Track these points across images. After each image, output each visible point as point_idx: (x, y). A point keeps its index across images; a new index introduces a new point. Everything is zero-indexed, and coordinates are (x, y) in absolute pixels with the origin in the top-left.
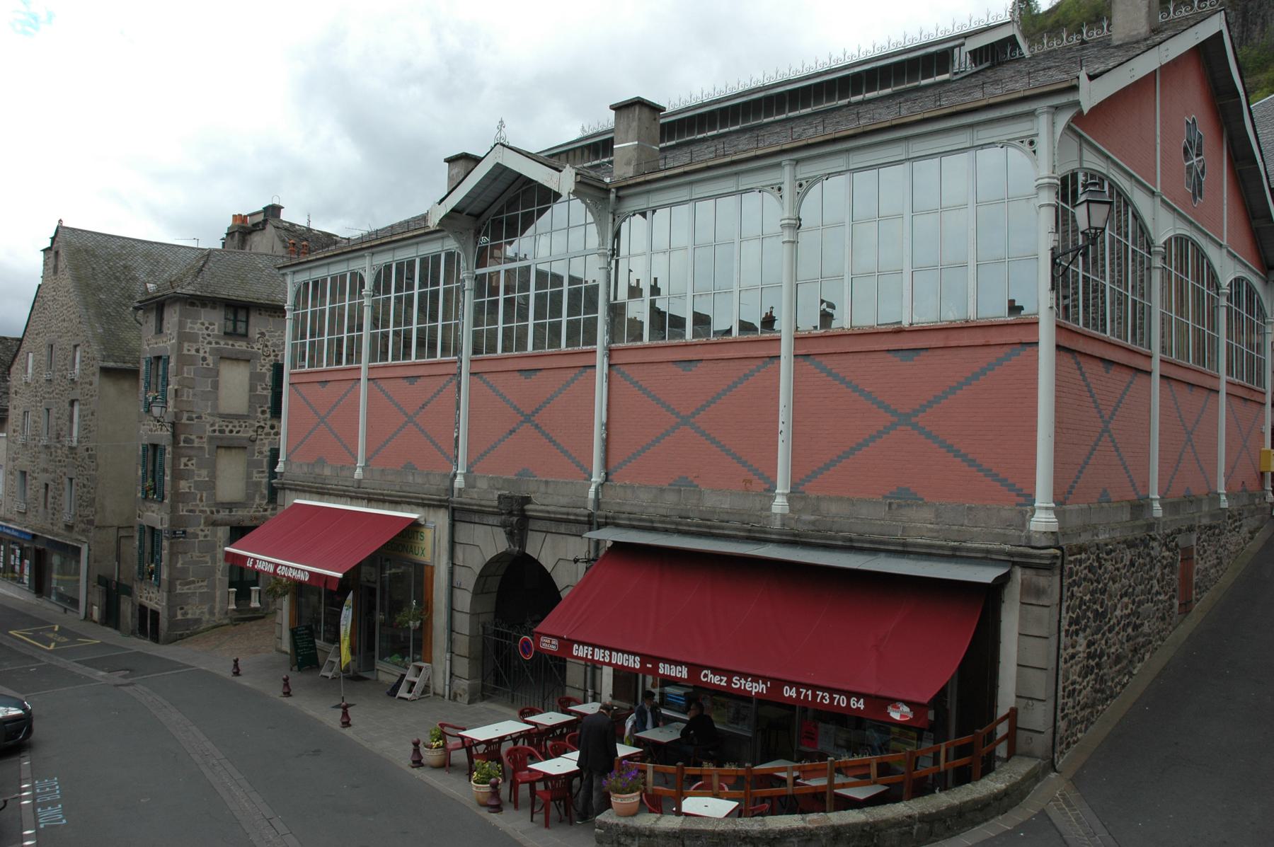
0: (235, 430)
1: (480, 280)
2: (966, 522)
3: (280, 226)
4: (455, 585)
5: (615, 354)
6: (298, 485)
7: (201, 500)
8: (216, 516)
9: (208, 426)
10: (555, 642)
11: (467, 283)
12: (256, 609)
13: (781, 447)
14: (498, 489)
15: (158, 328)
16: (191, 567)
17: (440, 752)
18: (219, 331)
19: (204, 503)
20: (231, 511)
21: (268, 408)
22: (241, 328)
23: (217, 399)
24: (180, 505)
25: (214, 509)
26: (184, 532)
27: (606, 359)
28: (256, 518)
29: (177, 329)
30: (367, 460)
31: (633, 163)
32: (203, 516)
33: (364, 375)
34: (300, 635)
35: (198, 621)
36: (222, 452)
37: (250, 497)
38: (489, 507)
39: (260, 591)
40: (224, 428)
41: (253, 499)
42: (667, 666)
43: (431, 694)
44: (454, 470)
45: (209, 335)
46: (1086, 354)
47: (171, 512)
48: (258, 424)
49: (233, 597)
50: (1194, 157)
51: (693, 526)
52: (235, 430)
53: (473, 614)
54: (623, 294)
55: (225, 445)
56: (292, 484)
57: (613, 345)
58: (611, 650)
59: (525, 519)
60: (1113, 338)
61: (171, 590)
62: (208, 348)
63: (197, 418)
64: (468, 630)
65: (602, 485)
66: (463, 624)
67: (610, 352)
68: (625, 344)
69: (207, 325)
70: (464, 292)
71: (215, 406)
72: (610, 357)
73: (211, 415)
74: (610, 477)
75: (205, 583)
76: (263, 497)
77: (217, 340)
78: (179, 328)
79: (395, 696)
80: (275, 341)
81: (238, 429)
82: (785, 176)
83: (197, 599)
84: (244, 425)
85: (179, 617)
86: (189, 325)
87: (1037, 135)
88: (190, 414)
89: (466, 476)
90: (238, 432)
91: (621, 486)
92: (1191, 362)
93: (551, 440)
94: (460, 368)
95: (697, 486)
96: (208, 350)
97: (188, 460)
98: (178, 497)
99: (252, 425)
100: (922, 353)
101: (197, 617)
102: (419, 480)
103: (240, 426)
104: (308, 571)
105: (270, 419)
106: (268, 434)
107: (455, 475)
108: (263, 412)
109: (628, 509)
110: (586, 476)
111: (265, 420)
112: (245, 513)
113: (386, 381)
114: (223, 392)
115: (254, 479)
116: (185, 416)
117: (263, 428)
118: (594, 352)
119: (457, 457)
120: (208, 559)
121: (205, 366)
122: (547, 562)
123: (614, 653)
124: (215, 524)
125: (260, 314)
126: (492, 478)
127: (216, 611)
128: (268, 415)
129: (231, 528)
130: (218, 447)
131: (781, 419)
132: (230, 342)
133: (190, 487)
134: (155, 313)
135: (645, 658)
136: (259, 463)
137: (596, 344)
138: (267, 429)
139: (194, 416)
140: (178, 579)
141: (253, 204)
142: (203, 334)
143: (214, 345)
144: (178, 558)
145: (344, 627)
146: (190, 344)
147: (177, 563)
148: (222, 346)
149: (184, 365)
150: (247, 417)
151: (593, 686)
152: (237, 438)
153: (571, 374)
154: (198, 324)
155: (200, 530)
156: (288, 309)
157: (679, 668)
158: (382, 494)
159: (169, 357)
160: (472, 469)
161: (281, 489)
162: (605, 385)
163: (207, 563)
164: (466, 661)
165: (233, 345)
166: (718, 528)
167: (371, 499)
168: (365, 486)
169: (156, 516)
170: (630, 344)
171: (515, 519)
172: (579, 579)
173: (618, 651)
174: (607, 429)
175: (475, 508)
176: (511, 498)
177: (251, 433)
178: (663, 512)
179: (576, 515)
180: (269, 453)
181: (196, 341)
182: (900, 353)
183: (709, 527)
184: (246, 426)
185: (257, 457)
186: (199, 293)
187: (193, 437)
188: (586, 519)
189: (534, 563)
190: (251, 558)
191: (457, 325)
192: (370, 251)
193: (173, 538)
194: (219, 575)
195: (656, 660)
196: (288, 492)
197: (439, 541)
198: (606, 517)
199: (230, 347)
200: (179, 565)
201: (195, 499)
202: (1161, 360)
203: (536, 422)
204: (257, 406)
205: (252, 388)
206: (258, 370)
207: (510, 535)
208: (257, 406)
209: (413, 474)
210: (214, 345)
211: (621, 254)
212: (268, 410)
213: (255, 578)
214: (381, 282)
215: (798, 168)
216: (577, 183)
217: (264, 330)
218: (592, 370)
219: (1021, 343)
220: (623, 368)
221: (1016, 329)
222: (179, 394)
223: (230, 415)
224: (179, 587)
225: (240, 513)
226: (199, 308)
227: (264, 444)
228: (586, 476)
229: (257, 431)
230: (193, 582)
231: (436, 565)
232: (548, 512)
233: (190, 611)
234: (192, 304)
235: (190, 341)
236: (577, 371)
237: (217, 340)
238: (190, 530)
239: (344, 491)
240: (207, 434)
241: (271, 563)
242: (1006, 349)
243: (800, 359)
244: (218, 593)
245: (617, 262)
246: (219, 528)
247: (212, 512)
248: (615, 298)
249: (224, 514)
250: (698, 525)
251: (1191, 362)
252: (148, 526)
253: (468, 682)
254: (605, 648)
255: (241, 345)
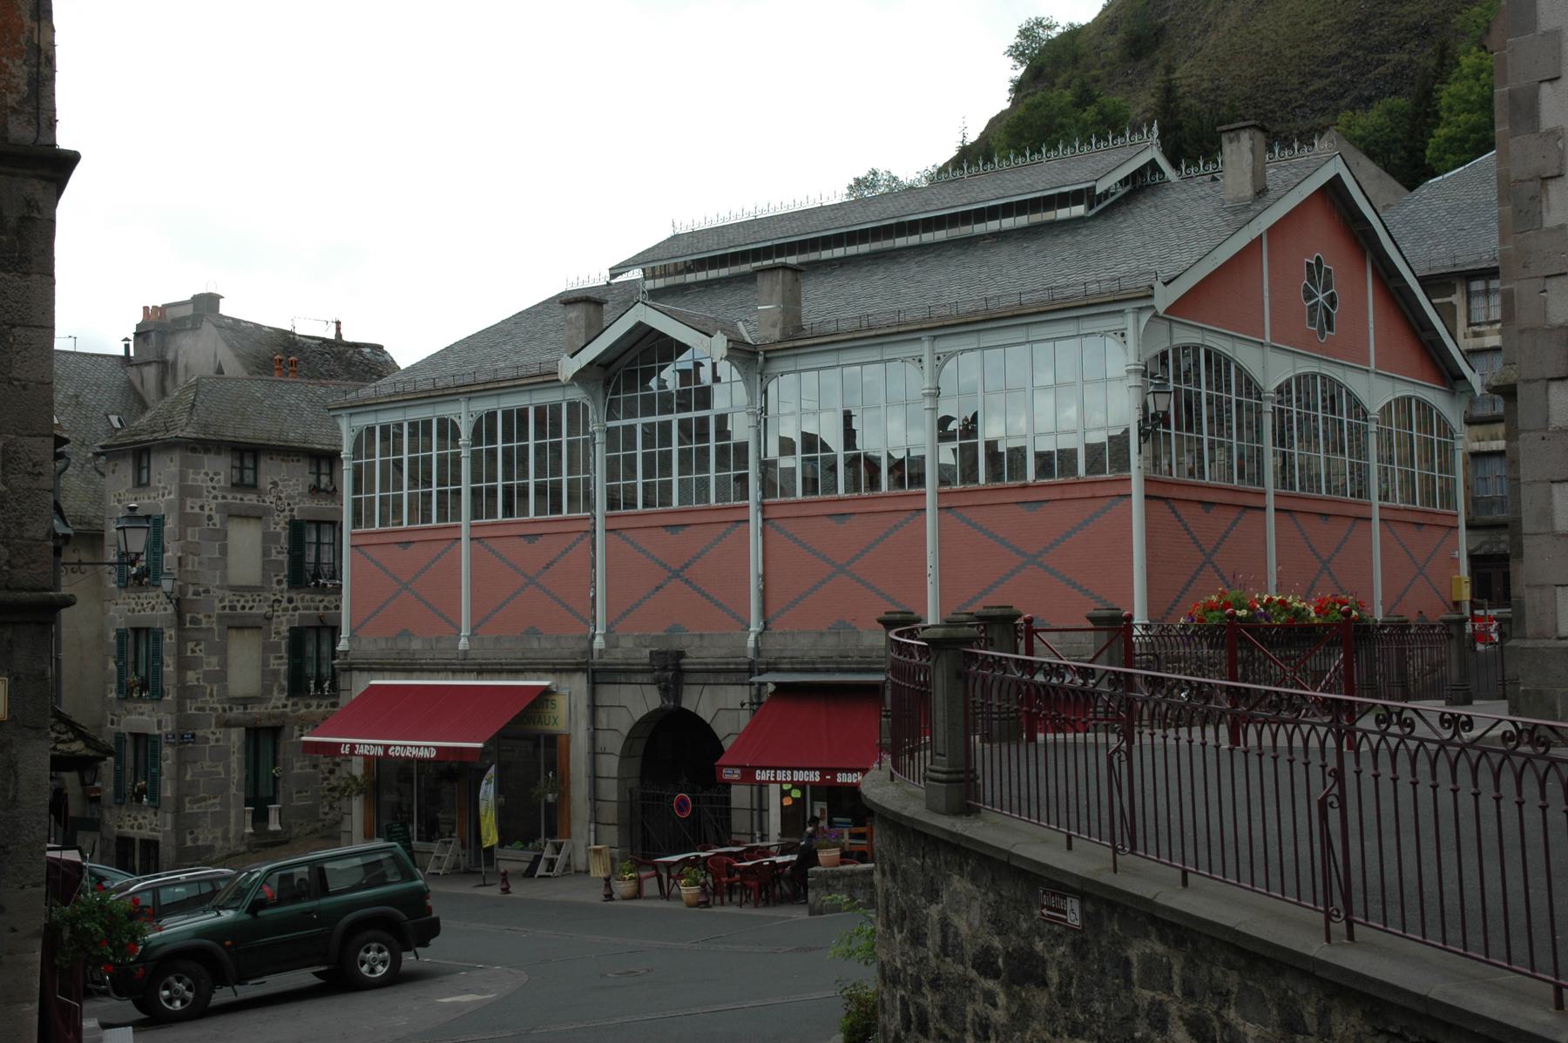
0: (248, 606)
1: (612, 434)
2: (1083, 640)
3: (223, 325)
4: (598, 750)
5: (769, 509)
6: (374, 663)
7: (211, 695)
8: (229, 715)
9: (217, 601)
10: (738, 771)
11: (597, 436)
12: (276, 833)
13: (930, 588)
14: (646, 647)
15: (136, 480)
16: (202, 780)
17: (632, 883)
18: (225, 482)
19: (215, 699)
20: (245, 708)
21: (285, 576)
22: (249, 476)
23: (226, 567)
24: (188, 701)
25: (227, 706)
26: (193, 736)
27: (759, 514)
28: (274, 716)
29: (178, 481)
30: (473, 629)
31: (779, 326)
32: (214, 715)
33: (465, 534)
34: (396, 832)
35: (210, 849)
36: (233, 633)
37: (267, 689)
38: (638, 665)
39: (280, 809)
40: (235, 603)
41: (271, 692)
42: (844, 774)
43: (573, 871)
44: (592, 630)
45: (214, 488)
46: (1179, 500)
47: (178, 711)
48: (273, 598)
49: (249, 817)
50: (1321, 300)
51: (854, 664)
52: (248, 606)
53: (621, 778)
54: (773, 451)
55: (238, 624)
56: (363, 664)
57: (766, 501)
58: (792, 769)
59: (680, 672)
60: (1213, 482)
61: (178, 810)
62: (213, 504)
63: (204, 592)
64: (616, 795)
65: (761, 633)
66: (610, 790)
67: (763, 507)
68: (778, 499)
69: (211, 475)
70: (594, 445)
71: (224, 577)
72: (763, 512)
73: (220, 587)
74: (769, 626)
75: (217, 801)
76: (281, 690)
77: (225, 494)
78: (181, 480)
79: (533, 876)
80: (289, 490)
81: (251, 604)
82: (925, 349)
83: (209, 821)
84: (257, 599)
85: (189, 844)
86: (191, 476)
87: (1126, 329)
88: (196, 588)
89: (606, 637)
90: (251, 608)
91: (780, 634)
92: (1324, 492)
93: (703, 594)
94: (594, 524)
95: (855, 628)
96: (214, 507)
97: (196, 645)
98: (185, 692)
99: (267, 599)
100: (1045, 505)
101: (209, 843)
102: (546, 645)
103: (254, 601)
104: (434, 747)
105: (288, 591)
106: (286, 609)
107: (593, 637)
108: (279, 582)
109: (789, 654)
110: (743, 626)
111: (282, 591)
112: (262, 710)
113: (496, 540)
114: (232, 559)
115: (271, 667)
116: (191, 589)
117: (280, 602)
118: (747, 507)
119: (595, 617)
120: (220, 769)
121: (211, 527)
122: (705, 713)
123: (795, 772)
124: (227, 724)
125: (271, 459)
126: (638, 637)
127: (231, 835)
128: (285, 586)
129: (248, 730)
130: (229, 628)
131: (929, 564)
132: (239, 496)
133: (198, 679)
134: (131, 461)
135: (823, 771)
136: (276, 647)
137: (748, 499)
138: (285, 604)
139: (201, 589)
140: (186, 795)
141: (177, 290)
142: (207, 487)
143: (220, 500)
144: (186, 769)
145: (485, 802)
146: (195, 500)
147: (186, 774)
148: (229, 500)
149: (187, 526)
150: (261, 588)
151: (761, 829)
152: (251, 616)
153: (723, 528)
154: (202, 475)
155: (210, 733)
156: (346, 458)
157: (855, 775)
158: (501, 664)
159: (164, 516)
160: (612, 629)
161: (345, 670)
162: (760, 538)
163: (220, 774)
164: (615, 829)
165: (242, 499)
166: (877, 663)
167: (481, 671)
168: (473, 656)
169: (145, 718)
170: (783, 499)
171: (671, 674)
172: (742, 728)
173: (798, 769)
174: (764, 580)
175: (621, 667)
176: (665, 653)
177: (266, 609)
178: (822, 653)
179: (736, 664)
180: (287, 634)
181: (200, 496)
182: (1025, 506)
183: (869, 663)
184: (260, 601)
185: (274, 638)
186: (203, 436)
187: (201, 616)
188: (747, 667)
189: (693, 719)
190: (346, 744)
191: (587, 481)
192: (468, 395)
193: (181, 744)
194: (233, 790)
195: (834, 771)
196: (355, 674)
197: (576, 707)
198: (768, 664)
199: (238, 501)
200: (188, 777)
201: (204, 694)
202: (1275, 495)
203: (687, 577)
204: (272, 574)
205: (266, 553)
206: (272, 529)
207: (664, 691)
208: (272, 574)
209: (539, 639)
210: (220, 500)
211: (769, 413)
212: (285, 580)
213: (271, 794)
214: (484, 428)
215: (936, 342)
216: (729, 349)
217: (276, 479)
218: (746, 525)
219: (1119, 496)
220: (777, 522)
221: (1115, 484)
222: (183, 562)
223: (242, 587)
224: (188, 805)
225: (256, 710)
226: (201, 455)
227: (282, 622)
228: (743, 626)
229: (273, 607)
230: (204, 799)
231: (572, 733)
232: (706, 664)
233: (201, 837)
234: (194, 450)
235: (192, 497)
236: (729, 525)
237: (225, 494)
238: (199, 733)
239: (445, 664)
240: (217, 611)
241: (378, 745)
242: (1108, 500)
243: (944, 511)
244: (233, 813)
245: (766, 420)
246: (233, 729)
247: (224, 710)
248: (766, 455)
249: (237, 712)
250: (859, 663)
251: (1324, 492)
252: (131, 734)
253: (617, 850)
254: (786, 769)
255: (250, 499)
